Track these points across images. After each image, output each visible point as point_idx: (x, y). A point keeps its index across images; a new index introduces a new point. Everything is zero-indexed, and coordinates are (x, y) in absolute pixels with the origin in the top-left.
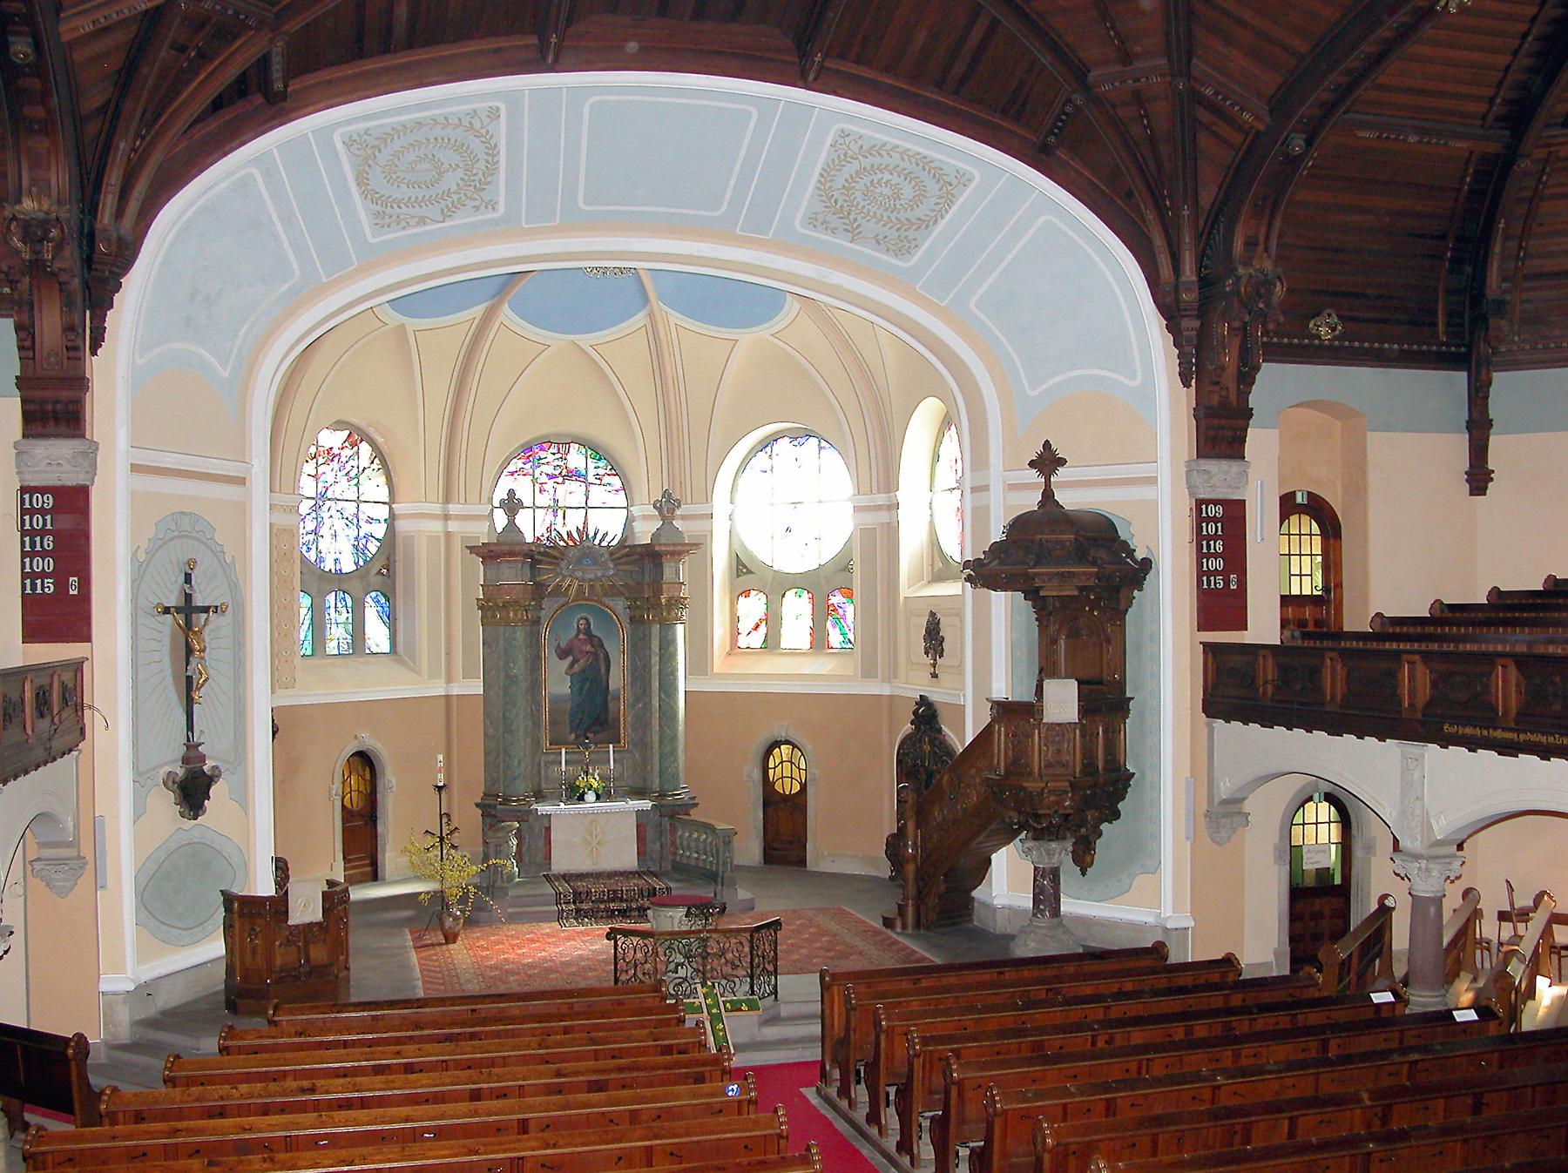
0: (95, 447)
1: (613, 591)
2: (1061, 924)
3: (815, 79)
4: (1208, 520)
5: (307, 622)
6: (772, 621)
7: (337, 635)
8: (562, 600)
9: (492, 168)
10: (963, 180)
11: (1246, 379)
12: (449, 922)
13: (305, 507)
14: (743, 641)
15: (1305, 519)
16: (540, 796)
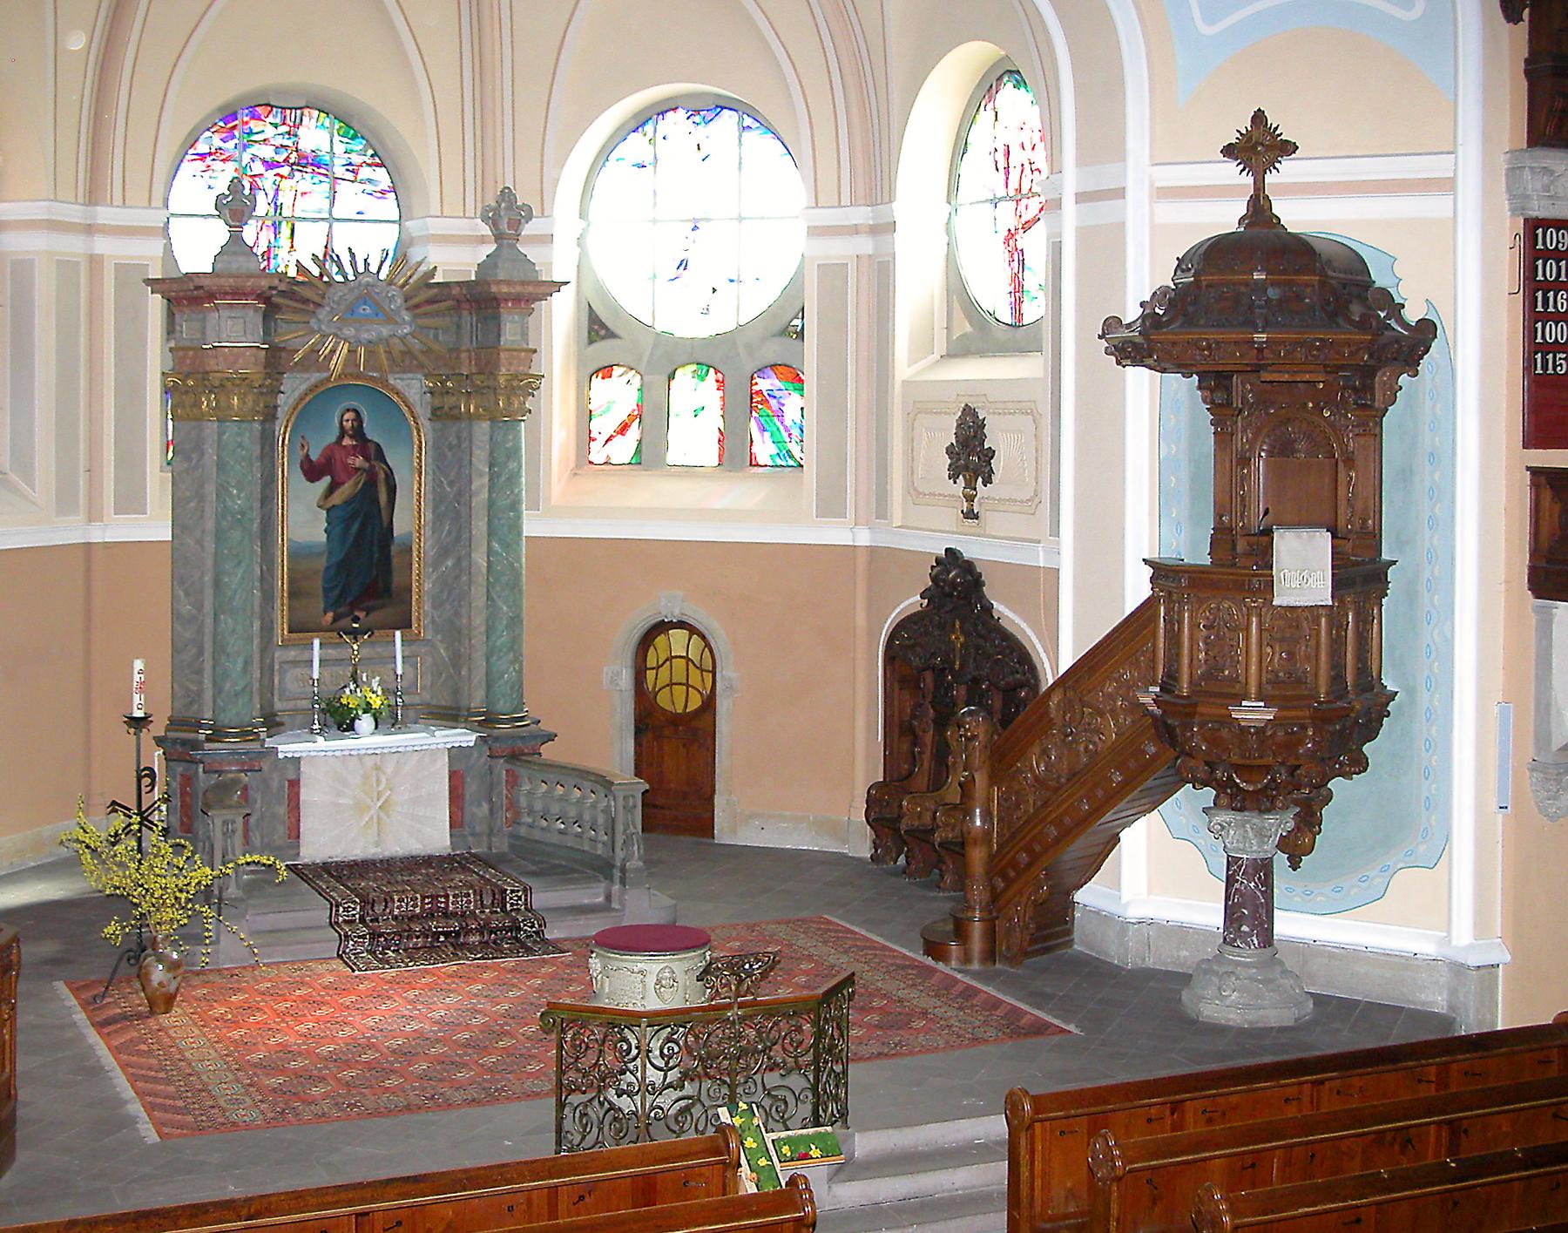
1: (406, 360)
2: (1273, 960)
6: (650, 419)
8: (316, 377)
12: (158, 973)
14: (597, 454)
16: (273, 723)
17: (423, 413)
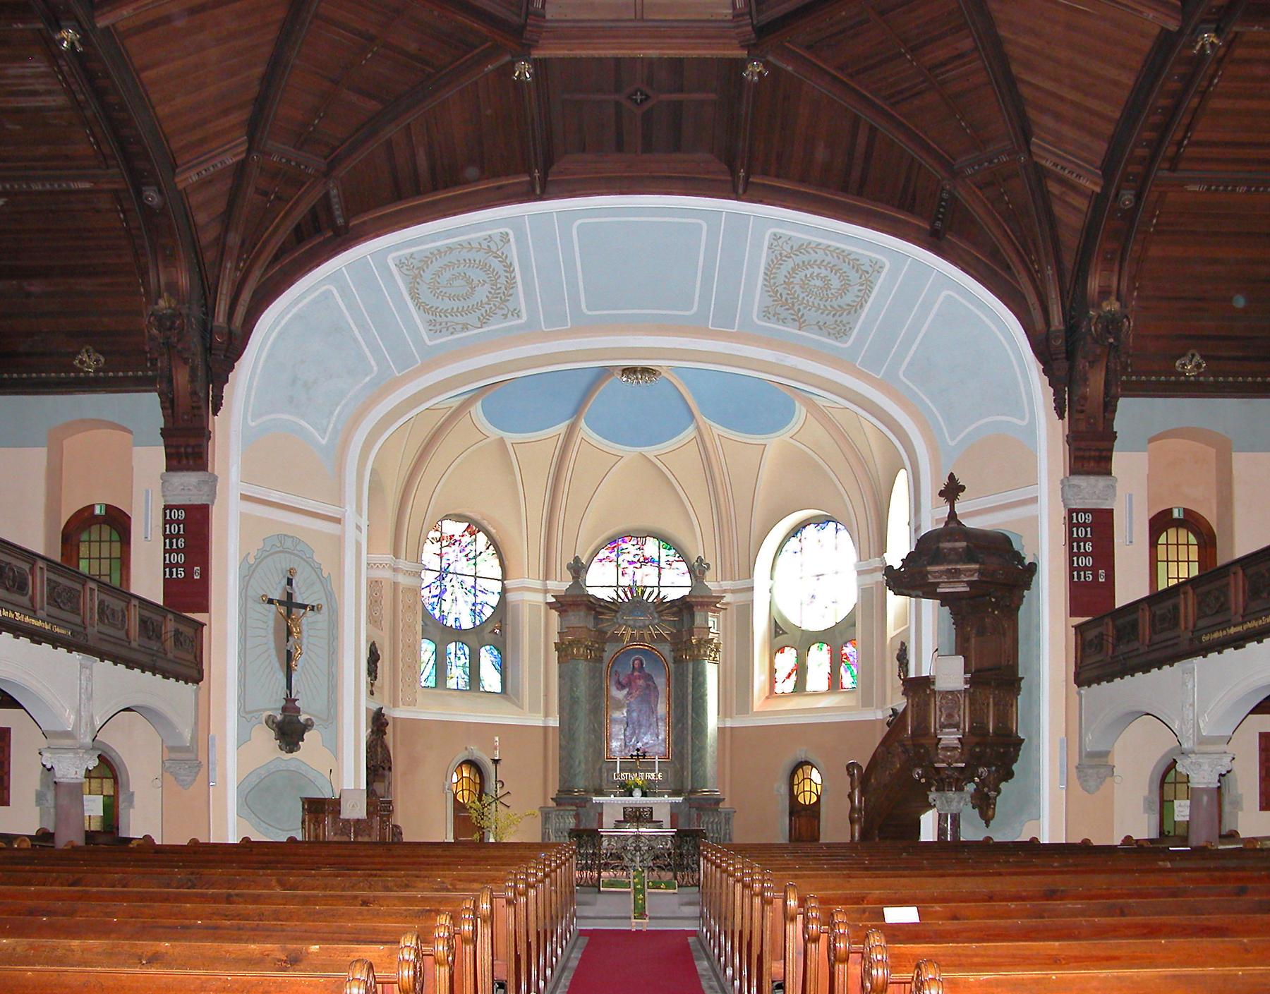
0: (215, 479)
3: (744, 192)
4: (1078, 525)
5: (432, 662)
6: (800, 670)
7: (457, 676)
9: (511, 284)
10: (877, 267)
11: (1109, 408)
13: (429, 577)
14: (779, 688)
15: (1183, 532)
16: (600, 793)
17: (670, 660)
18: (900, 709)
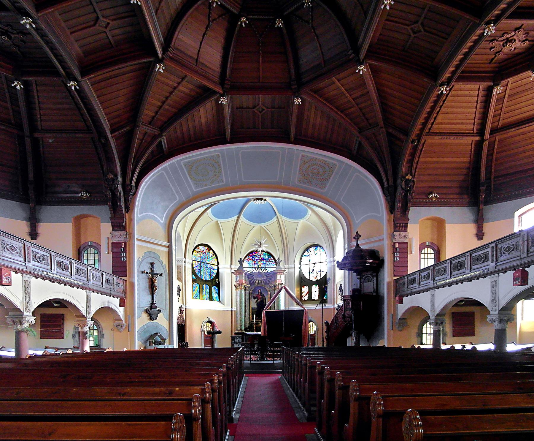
6: (310, 292)
10: (334, 166)
15: (429, 249)
18: (341, 305)
